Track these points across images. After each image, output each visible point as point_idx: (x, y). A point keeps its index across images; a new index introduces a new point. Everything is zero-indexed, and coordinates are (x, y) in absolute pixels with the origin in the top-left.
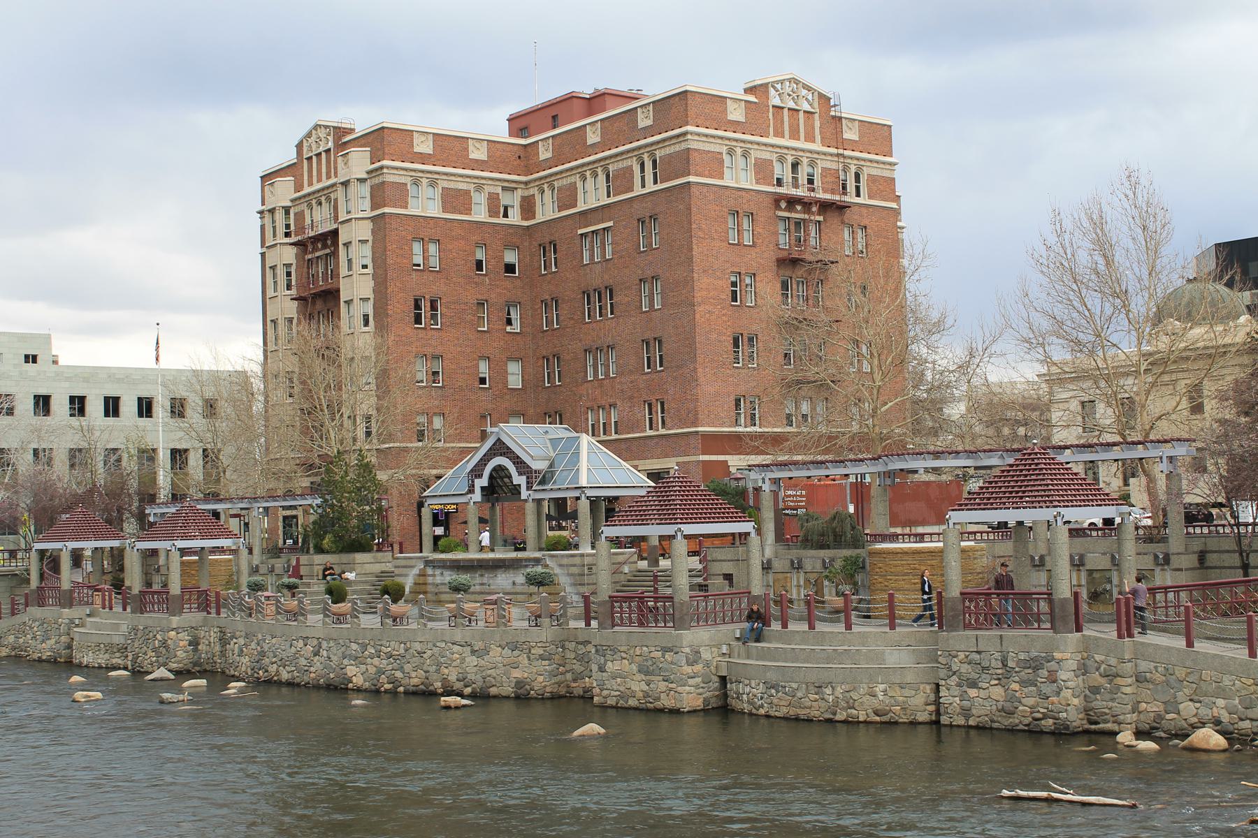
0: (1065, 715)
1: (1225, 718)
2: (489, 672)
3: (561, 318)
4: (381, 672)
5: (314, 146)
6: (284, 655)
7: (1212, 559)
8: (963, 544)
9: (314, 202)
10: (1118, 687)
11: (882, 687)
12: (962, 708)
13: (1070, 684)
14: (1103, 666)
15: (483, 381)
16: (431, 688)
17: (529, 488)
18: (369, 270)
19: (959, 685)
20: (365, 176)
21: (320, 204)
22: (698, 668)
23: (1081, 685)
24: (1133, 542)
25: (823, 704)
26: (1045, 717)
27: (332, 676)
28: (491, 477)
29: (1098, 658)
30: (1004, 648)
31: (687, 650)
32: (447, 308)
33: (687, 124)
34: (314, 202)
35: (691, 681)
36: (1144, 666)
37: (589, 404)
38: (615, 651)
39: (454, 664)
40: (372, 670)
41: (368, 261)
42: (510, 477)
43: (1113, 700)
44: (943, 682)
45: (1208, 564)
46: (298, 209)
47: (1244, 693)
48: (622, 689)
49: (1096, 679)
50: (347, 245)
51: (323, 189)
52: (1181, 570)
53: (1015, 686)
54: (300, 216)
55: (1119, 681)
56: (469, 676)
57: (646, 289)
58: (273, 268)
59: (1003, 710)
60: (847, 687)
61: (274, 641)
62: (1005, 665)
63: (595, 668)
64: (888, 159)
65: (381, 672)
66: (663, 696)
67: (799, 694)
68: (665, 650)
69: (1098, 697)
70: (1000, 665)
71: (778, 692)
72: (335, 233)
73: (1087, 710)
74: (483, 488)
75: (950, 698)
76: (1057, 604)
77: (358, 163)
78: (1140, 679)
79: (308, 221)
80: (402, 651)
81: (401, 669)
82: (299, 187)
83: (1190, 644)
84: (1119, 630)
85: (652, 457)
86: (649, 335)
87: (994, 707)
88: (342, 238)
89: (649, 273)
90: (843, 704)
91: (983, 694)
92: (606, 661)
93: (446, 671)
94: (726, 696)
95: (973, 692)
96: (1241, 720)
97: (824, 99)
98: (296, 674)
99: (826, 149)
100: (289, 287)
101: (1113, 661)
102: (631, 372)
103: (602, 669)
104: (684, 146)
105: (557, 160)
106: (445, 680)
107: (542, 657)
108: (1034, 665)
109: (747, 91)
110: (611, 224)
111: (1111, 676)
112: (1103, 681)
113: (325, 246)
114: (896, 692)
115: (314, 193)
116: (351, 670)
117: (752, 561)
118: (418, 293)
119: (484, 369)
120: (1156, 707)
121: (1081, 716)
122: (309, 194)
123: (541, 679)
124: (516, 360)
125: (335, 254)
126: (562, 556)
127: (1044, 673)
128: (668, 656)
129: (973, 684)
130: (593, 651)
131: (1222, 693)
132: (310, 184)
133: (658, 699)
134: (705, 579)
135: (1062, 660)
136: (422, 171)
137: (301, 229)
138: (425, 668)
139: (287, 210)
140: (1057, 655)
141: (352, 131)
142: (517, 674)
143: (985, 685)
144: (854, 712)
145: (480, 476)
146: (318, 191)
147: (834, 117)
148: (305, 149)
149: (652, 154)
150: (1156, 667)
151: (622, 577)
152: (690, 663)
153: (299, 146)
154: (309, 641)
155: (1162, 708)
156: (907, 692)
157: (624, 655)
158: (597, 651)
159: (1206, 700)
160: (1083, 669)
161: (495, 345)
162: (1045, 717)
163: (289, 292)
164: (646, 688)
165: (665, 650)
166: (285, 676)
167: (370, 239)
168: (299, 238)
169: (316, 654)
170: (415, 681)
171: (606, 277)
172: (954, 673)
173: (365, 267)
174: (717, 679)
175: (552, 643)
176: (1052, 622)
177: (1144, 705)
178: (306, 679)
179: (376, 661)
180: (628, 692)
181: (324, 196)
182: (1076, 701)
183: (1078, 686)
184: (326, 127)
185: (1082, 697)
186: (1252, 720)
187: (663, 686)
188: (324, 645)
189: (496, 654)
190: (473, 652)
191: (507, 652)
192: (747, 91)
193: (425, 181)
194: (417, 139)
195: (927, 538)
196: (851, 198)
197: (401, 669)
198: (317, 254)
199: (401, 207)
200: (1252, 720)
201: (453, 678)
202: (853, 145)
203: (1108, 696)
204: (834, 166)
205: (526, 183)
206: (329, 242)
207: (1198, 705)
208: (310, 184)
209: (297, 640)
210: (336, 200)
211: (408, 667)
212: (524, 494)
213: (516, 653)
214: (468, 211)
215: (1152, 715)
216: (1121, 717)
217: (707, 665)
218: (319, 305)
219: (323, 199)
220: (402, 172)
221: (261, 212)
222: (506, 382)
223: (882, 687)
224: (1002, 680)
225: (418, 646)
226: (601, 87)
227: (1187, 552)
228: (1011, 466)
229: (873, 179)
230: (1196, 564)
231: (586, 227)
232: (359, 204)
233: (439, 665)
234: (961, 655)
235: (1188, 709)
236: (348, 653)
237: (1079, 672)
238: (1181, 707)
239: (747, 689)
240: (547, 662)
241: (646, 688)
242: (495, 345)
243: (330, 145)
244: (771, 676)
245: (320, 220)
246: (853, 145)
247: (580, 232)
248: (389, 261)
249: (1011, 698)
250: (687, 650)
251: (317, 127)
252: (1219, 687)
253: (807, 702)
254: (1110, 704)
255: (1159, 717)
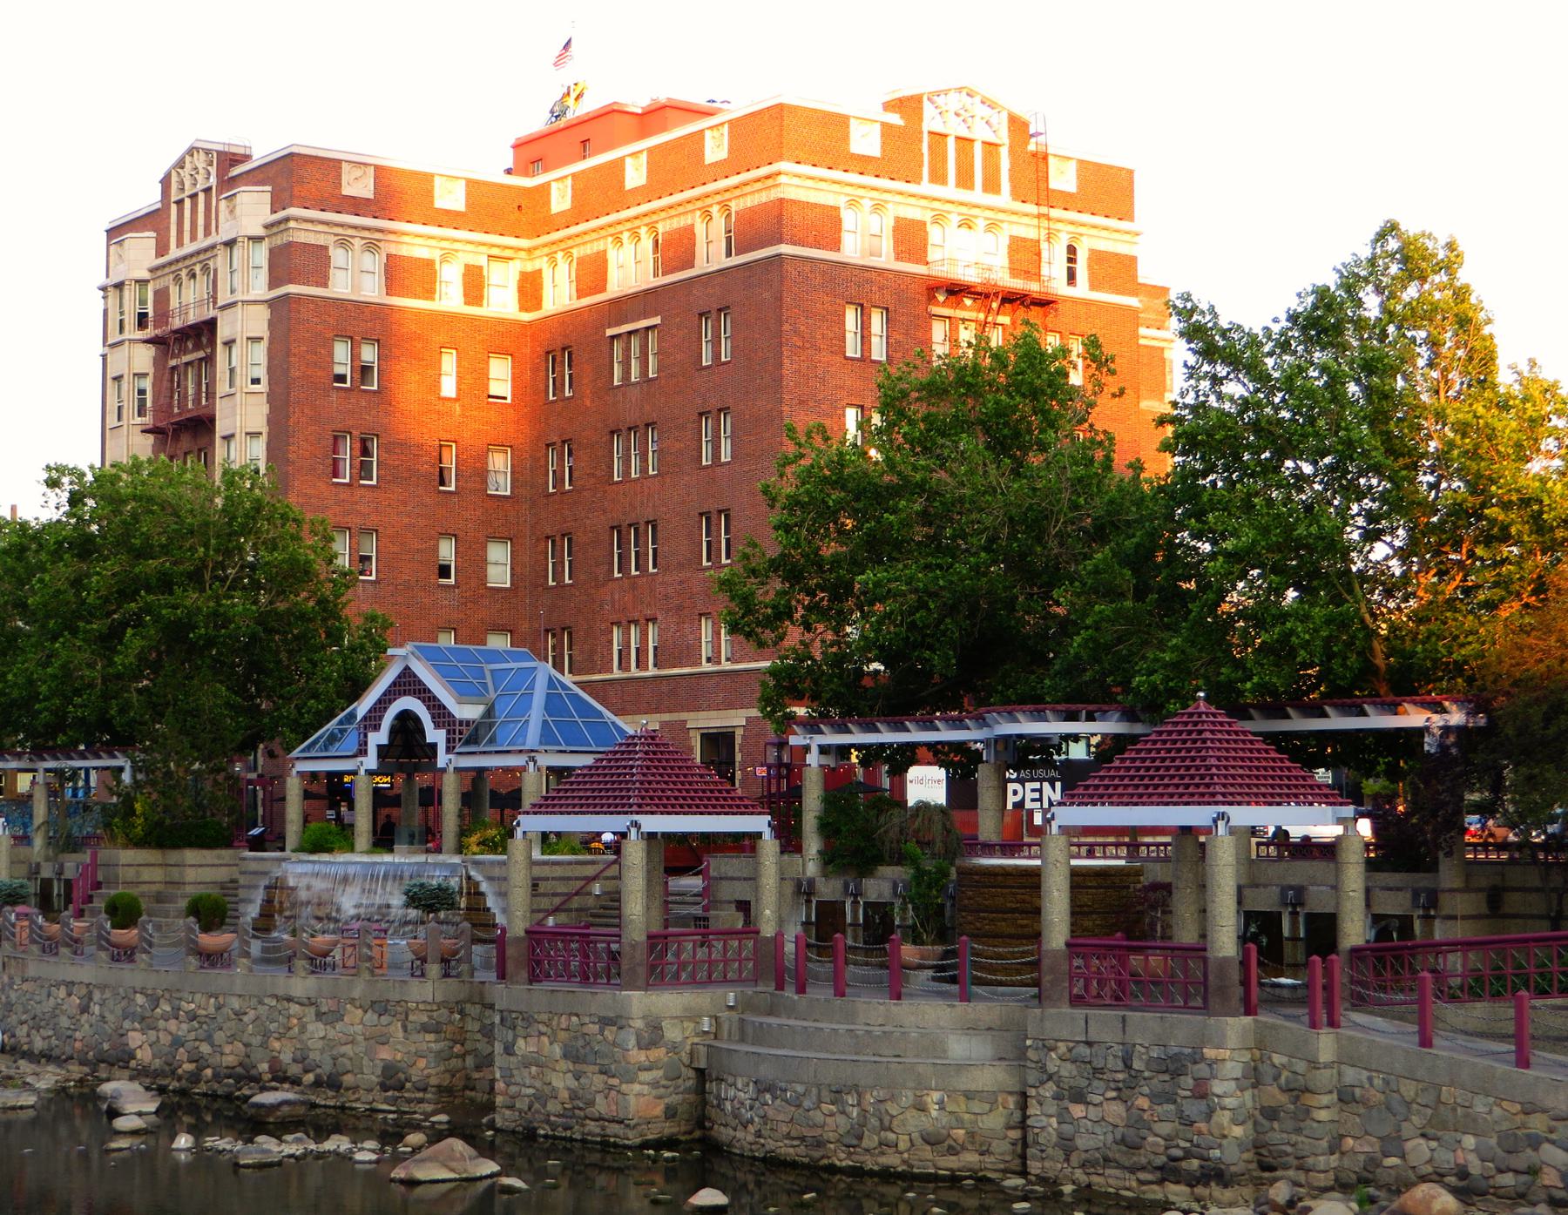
0: (1217, 1153)
1: (1475, 1166)
2: (344, 1049)
3: (576, 474)
4: (177, 1042)
5: (187, 184)
6: (39, 1010)
7: (1513, 902)
8: (1074, 862)
9: (184, 273)
10: (1308, 1111)
11: (936, 1096)
12: (1061, 1137)
13: (1228, 1102)
14: (1285, 1074)
15: (444, 571)
16: (253, 1072)
17: (449, 750)
18: (263, 387)
19: (1058, 1097)
20: (260, 232)
21: (194, 276)
22: (659, 1053)
23: (1249, 1104)
24: (1361, 868)
25: (841, 1119)
26: (1188, 1155)
27: (106, 1046)
28: (393, 732)
29: (1278, 1059)
30: (1128, 1040)
31: (639, 1024)
32: (388, 451)
33: (780, 158)
34: (184, 273)
35: (645, 1076)
36: (1351, 1075)
37: (614, 617)
38: (529, 1020)
39: (290, 1034)
40: (165, 1039)
41: (261, 372)
42: (422, 732)
43: (1298, 1131)
44: (1032, 1092)
45: (1507, 910)
46: (160, 284)
47: (1505, 1126)
48: (538, 1084)
49: (1273, 1095)
50: (229, 344)
51: (198, 253)
52: (1454, 918)
53: (1143, 1102)
54: (162, 296)
55: (1308, 1099)
56: (312, 1055)
57: (706, 426)
58: (118, 379)
59: (1123, 1141)
60: (882, 1094)
61: (25, 986)
62: (1128, 1066)
63: (498, 1048)
64: (1124, 225)
65: (177, 1042)
66: (599, 1099)
67: (807, 1104)
68: (605, 1022)
69: (1276, 1125)
70: (1120, 1065)
71: (774, 1098)
72: (211, 325)
73: (1257, 1146)
74: (380, 747)
75: (1044, 1120)
76: (1211, 967)
77: (251, 210)
78: (1346, 1097)
79: (174, 303)
80: (212, 1010)
81: (209, 1039)
82: (162, 249)
83: (1426, 1042)
84: (1312, 1014)
85: (709, 708)
86: (711, 506)
87: (1110, 1138)
88: (222, 333)
89: (714, 403)
90: (874, 1122)
91: (1093, 1113)
92: (516, 1037)
93: (277, 1045)
94: (704, 1103)
95: (1078, 1110)
96: (1501, 1171)
97: (1018, 127)
98: (54, 1041)
99: (1018, 206)
100: (141, 411)
101: (1301, 1066)
102: (681, 566)
103: (509, 1050)
104: (774, 194)
105: (580, 212)
106: (274, 1062)
107: (425, 1028)
108: (1173, 1067)
109: (888, 106)
110: (657, 320)
111: (1298, 1091)
112: (1283, 1098)
113: (197, 347)
114: (960, 1106)
115: (185, 258)
116: (135, 1039)
117: (764, 880)
118: (340, 426)
119: (447, 551)
120: (1369, 1146)
121: (1246, 1156)
122: (177, 261)
123: (422, 1063)
124: (502, 539)
125: (210, 360)
126: (492, 863)
127: (1188, 1081)
128: (609, 1033)
129: (1079, 1097)
130: (497, 1019)
131: (1470, 1124)
132: (180, 244)
133: (592, 1103)
134: (706, 909)
135: (1216, 1061)
136: (355, 227)
137: (163, 314)
138: (245, 1040)
139: (142, 283)
140: (1209, 1053)
141: (247, 158)
142: (385, 1054)
143: (1097, 1099)
144: (892, 1136)
145: (377, 728)
146: (192, 255)
147: (1034, 155)
148: (174, 186)
149: (725, 206)
150: (1370, 1079)
151: (590, 902)
152: (642, 1046)
153: (166, 182)
154: (75, 989)
155: (1377, 1148)
156: (977, 1107)
157: (543, 1029)
158: (502, 1020)
159: (1448, 1136)
160: (1254, 1077)
161: (467, 515)
162: (1188, 1155)
163: (139, 420)
164: (573, 1084)
165: (605, 1022)
166: (39, 1044)
167: (266, 335)
168: (158, 332)
169: (85, 1009)
170: (230, 1060)
171: (647, 408)
172: (1050, 1078)
173: (256, 381)
174: (692, 1073)
175: (440, 1005)
176: (1205, 1000)
177: (1350, 1141)
178: (68, 1049)
179: (172, 1025)
180: (547, 1089)
181: (198, 264)
182: (1238, 1131)
183: (1243, 1105)
184: (208, 152)
185: (1250, 1124)
186: (1516, 1172)
187: (598, 1081)
188: (97, 996)
189: (356, 1021)
190: (319, 1016)
191: (371, 1017)
192: (888, 106)
193: (357, 243)
194: (347, 174)
195: (1098, 851)
196: (1060, 287)
197: (209, 1039)
198: (186, 359)
199: (318, 284)
200: (1516, 1172)
201: (286, 1057)
202: (1066, 201)
203: (1290, 1124)
204: (1031, 234)
205: (529, 250)
206: (204, 340)
207: (1434, 1144)
208: (180, 244)
209: (57, 985)
210: (215, 271)
211: (219, 1037)
212: (442, 759)
213: (385, 1019)
214: (429, 293)
215: (1362, 1158)
216: (1311, 1161)
217: (674, 1048)
218: (185, 442)
219: (197, 268)
220: (320, 228)
221: (104, 289)
222: (483, 577)
223: (936, 1096)
224: (1123, 1093)
225: (236, 1003)
226: (663, 98)
227: (1467, 889)
228: (590, 768)
229: (1097, 257)
230: (1484, 910)
231: (618, 324)
232: (249, 279)
233: (266, 1035)
234: (1062, 1047)
235: (1420, 1150)
236: (131, 1009)
237: (1246, 1083)
238: (1409, 1145)
239: (731, 1092)
240: (431, 1037)
241: (573, 1084)
242: (467, 515)
243: (213, 181)
244: (766, 1072)
245: (188, 303)
246: (1066, 201)
247: (610, 332)
248: (295, 373)
249: (1138, 1122)
250: (639, 1024)
251: (192, 151)
252: (1467, 1115)
253: (817, 1117)
254: (1294, 1138)
255: (1373, 1163)
